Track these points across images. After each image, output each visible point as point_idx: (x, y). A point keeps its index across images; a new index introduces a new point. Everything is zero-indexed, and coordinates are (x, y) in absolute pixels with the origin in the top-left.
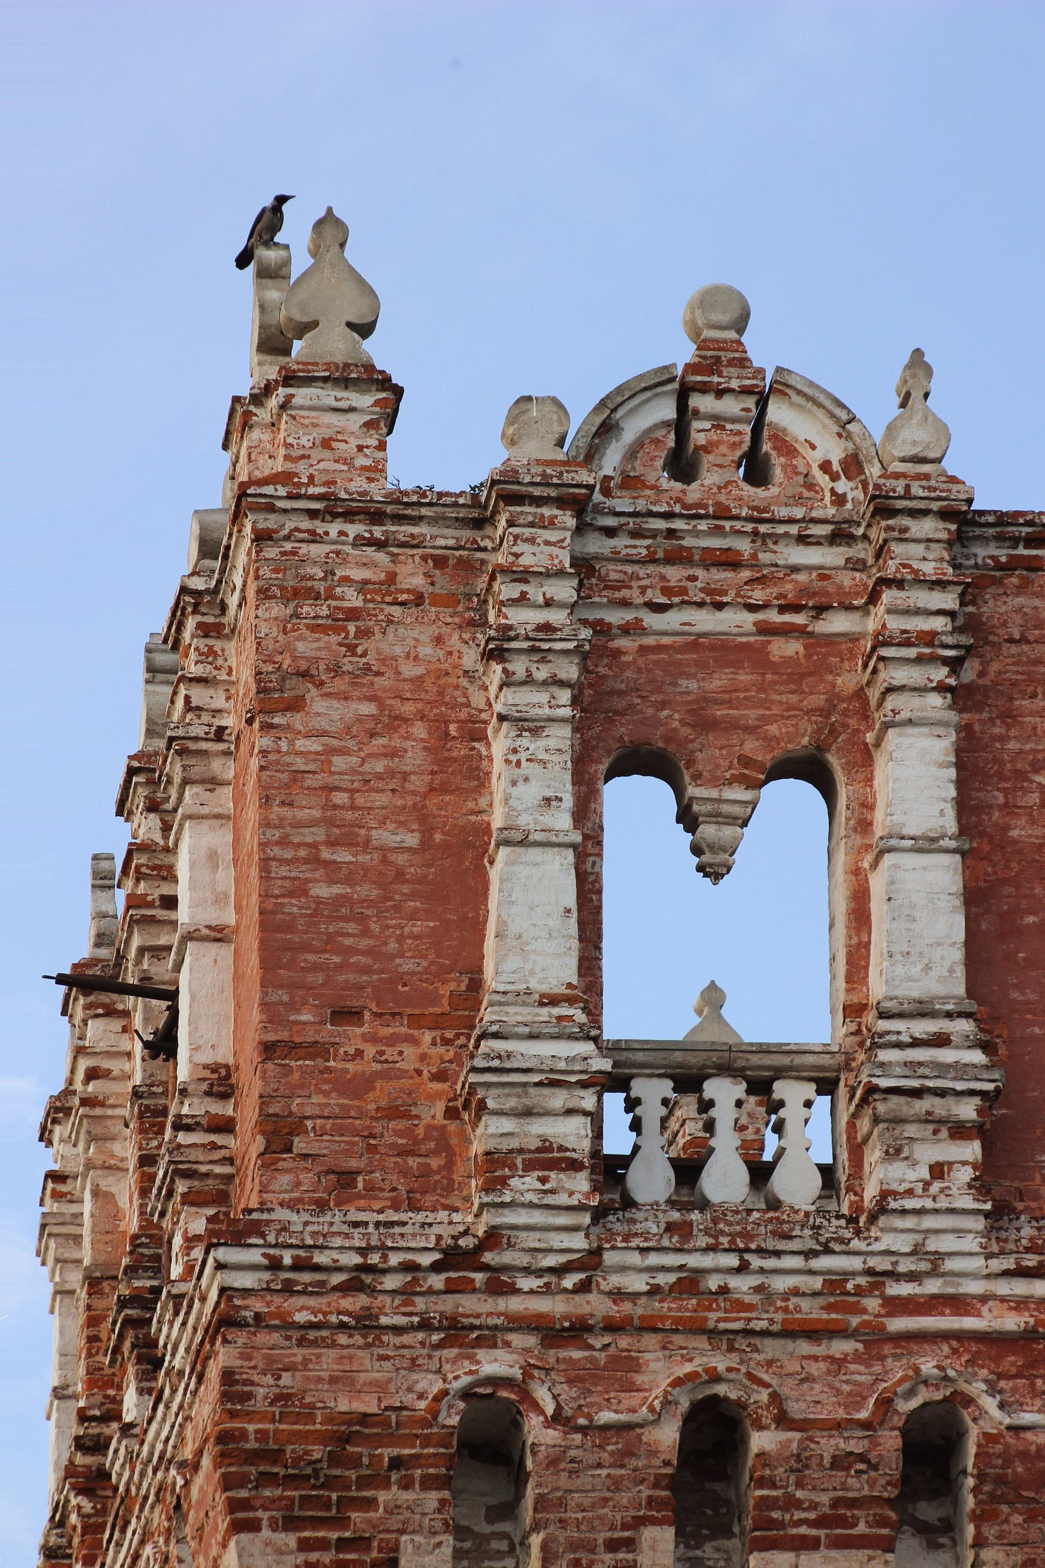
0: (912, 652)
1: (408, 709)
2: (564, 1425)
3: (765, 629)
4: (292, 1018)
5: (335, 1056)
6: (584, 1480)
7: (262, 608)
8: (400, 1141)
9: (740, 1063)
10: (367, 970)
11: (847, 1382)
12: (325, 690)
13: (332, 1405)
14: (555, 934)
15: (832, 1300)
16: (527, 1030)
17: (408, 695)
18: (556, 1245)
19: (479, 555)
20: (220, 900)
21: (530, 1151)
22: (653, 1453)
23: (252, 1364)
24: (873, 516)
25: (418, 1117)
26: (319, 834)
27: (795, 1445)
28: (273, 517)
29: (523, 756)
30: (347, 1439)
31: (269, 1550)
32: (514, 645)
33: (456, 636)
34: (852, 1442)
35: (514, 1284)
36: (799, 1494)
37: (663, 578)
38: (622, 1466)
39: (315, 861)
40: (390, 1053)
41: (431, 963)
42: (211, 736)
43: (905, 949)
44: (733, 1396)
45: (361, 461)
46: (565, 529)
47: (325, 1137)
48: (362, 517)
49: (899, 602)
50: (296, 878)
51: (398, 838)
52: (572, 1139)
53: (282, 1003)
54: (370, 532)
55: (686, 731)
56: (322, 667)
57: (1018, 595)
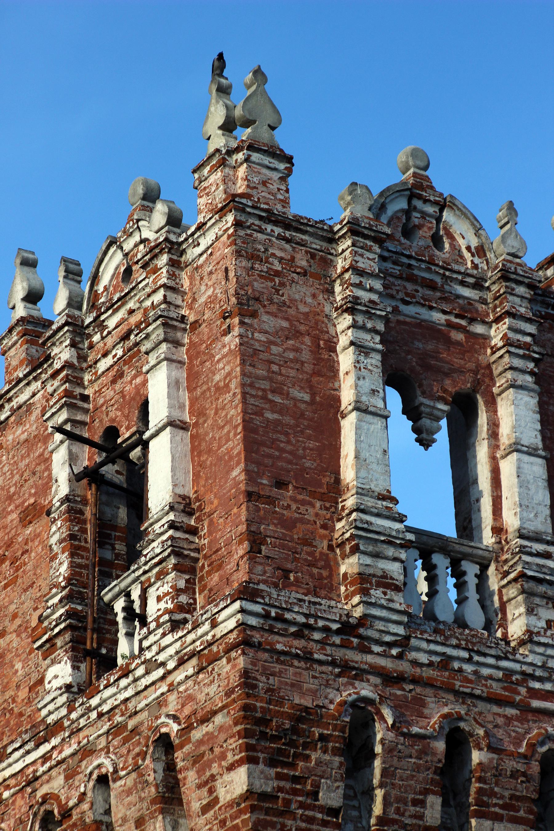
0: (521, 352)
1: (302, 328)
2: (397, 731)
3: (449, 324)
4: (259, 481)
5: (278, 505)
6: (403, 763)
7: (238, 260)
8: (309, 558)
9: (450, 548)
10: (290, 462)
11: (514, 731)
12: (266, 310)
13: (291, 699)
14: (380, 462)
15: (506, 685)
16: (376, 511)
17: (302, 321)
18: (392, 630)
19: (330, 257)
20: (182, 407)
21: (378, 577)
22: (434, 754)
23: (257, 668)
24: (499, 279)
25: (316, 547)
26: (265, 385)
27: (495, 761)
28: (243, 215)
29: (362, 366)
30: (299, 719)
31: (262, 776)
32: (359, 307)
33: (321, 296)
34: (520, 765)
35: (370, 648)
36: (496, 789)
37: (405, 288)
38: (421, 759)
39: (264, 398)
40: (302, 509)
41: (318, 465)
42: (179, 319)
43: (527, 504)
44: (467, 729)
45: (280, 197)
46: (375, 253)
47: (276, 549)
48: (281, 225)
49: (514, 325)
50: (258, 406)
51: (301, 395)
52: (396, 574)
53: (253, 471)
54: (284, 233)
55: (418, 368)
56: (265, 298)
57: (549, 333)
